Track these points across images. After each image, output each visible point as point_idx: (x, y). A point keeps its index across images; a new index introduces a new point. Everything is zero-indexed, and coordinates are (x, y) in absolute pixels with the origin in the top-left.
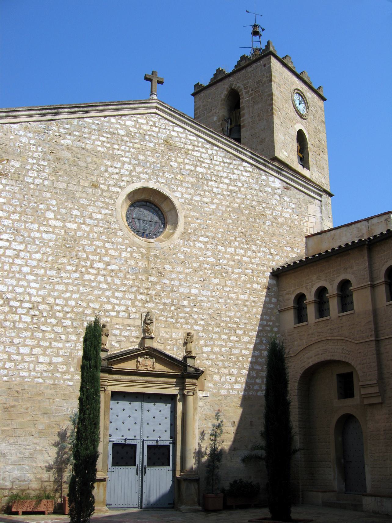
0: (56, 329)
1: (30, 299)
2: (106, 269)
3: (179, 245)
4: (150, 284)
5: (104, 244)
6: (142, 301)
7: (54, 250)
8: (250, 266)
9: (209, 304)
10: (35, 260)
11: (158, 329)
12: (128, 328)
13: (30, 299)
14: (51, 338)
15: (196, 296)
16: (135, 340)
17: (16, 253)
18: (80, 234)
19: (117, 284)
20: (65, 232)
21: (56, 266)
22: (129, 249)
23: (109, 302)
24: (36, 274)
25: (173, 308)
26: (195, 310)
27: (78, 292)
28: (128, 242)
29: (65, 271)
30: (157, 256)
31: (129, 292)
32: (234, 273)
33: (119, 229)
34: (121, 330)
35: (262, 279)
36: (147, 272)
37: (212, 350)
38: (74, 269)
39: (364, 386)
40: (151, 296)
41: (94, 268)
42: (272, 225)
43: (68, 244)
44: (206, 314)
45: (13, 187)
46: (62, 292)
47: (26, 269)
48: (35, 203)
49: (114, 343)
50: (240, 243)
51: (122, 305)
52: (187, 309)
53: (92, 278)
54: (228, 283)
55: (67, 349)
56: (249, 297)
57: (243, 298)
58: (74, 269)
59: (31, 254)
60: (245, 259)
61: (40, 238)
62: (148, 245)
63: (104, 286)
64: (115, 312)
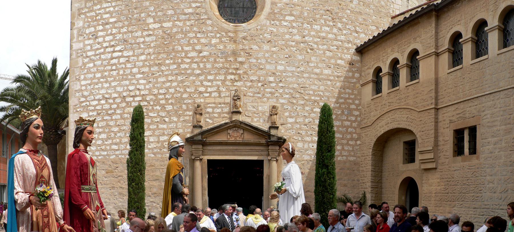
0: (160, 114)
1: (140, 93)
2: (198, 57)
3: (265, 25)
4: (238, 64)
5: (196, 35)
6: (231, 81)
7: (155, 49)
8: (335, 43)
9: (294, 79)
10: (141, 61)
11: (246, 104)
12: (219, 106)
13: (140, 93)
14: (158, 122)
15: (281, 72)
16: (226, 115)
17: (127, 59)
18: (175, 30)
19: (208, 69)
20: (164, 32)
21: (157, 62)
22: (218, 35)
23: (203, 85)
24: (143, 72)
25: (260, 84)
26: (281, 85)
27: (176, 81)
28: (217, 29)
29: (165, 65)
30: (244, 38)
31: (220, 74)
32: (319, 49)
33: (209, 19)
34: (213, 108)
35: (346, 55)
36: (235, 54)
37: (296, 120)
38: (172, 61)
39: (422, 152)
40: (239, 75)
41: (188, 58)
42: (359, 4)
43: (166, 41)
44: (291, 88)
45: (120, 7)
46: (164, 83)
47: (135, 70)
48: (137, 14)
49: (208, 120)
50: (325, 20)
51: (214, 86)
52: (274, 85)
53: (187, 66)
54: (313, 59)
55: (170, 129)
56: (333, 72)
57: (327, 73)
58: (172, 61)
59: (138, 57)
60: (330, 36)
61: (143, 42)
62: (235, 29)
63: (198, 72)
64: (207, 93)
